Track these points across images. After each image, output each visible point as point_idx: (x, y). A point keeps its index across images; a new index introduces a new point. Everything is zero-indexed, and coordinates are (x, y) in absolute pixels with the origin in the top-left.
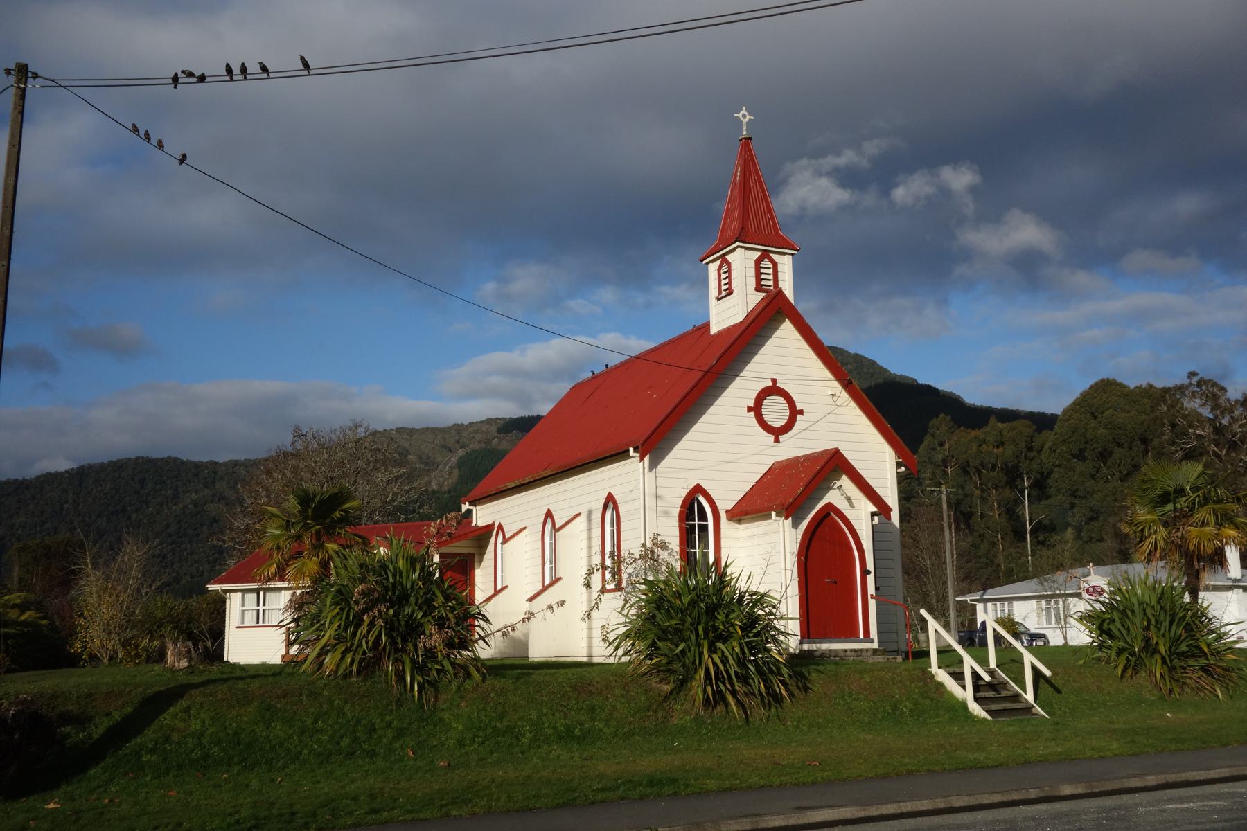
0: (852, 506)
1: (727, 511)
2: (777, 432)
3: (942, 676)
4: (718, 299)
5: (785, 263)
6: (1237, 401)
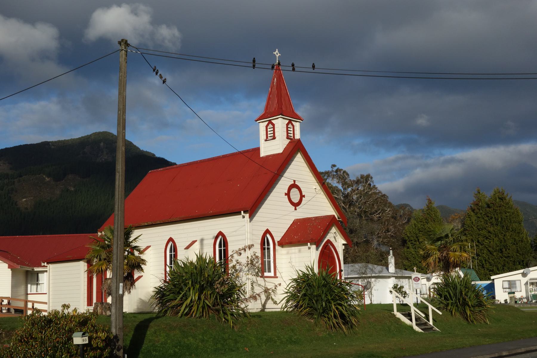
1: (278, 242)
2: (296, 205)
3: (399, 315)
4: (266, 140)
5: (297, 125)
6: (354, 181)
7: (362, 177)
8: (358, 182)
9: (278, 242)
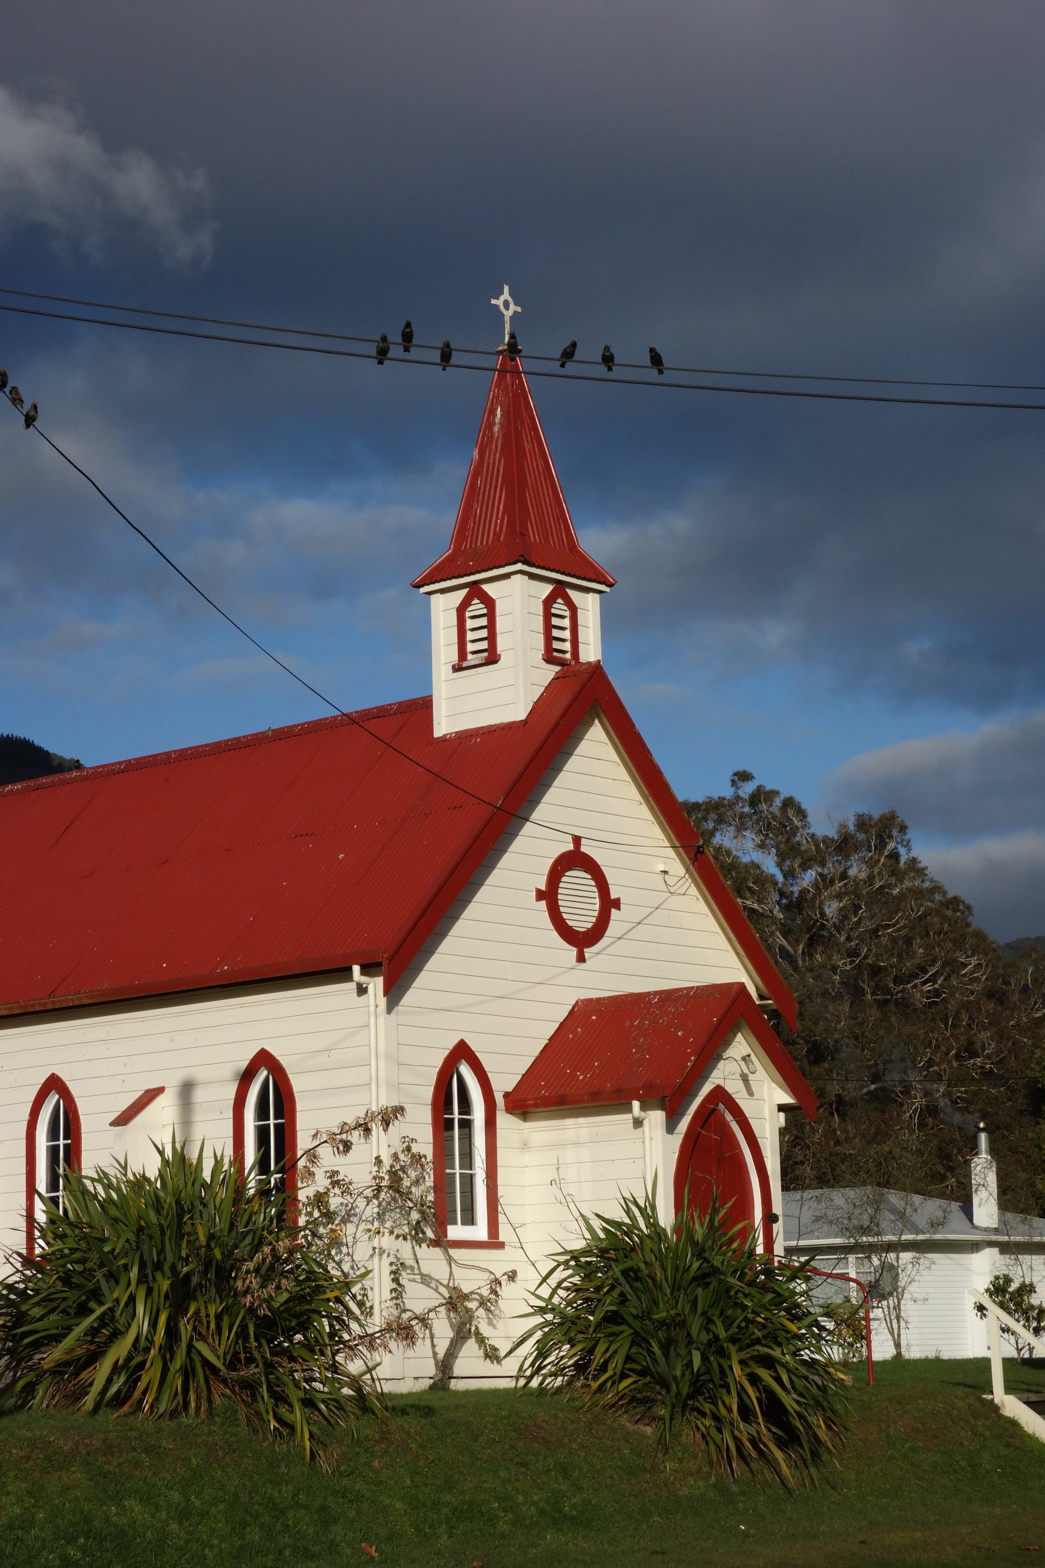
0: (751, 1093)
1: (507, 1095)
2: (583, 941)
4: (457, 668)
5: (589, 606)
7: (863, 823)
8: (844, 845)
9: (507, 1095)
